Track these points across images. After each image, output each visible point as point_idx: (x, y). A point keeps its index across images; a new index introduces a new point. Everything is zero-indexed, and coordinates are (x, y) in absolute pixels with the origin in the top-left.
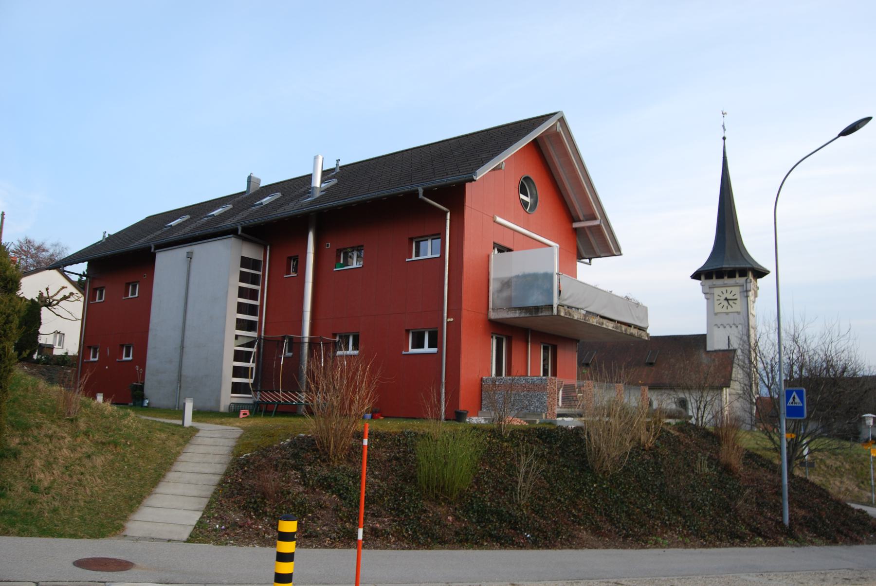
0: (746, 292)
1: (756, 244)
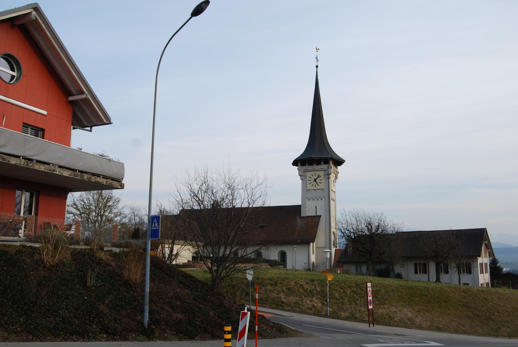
0: (328, 175)
1: (336, 141)
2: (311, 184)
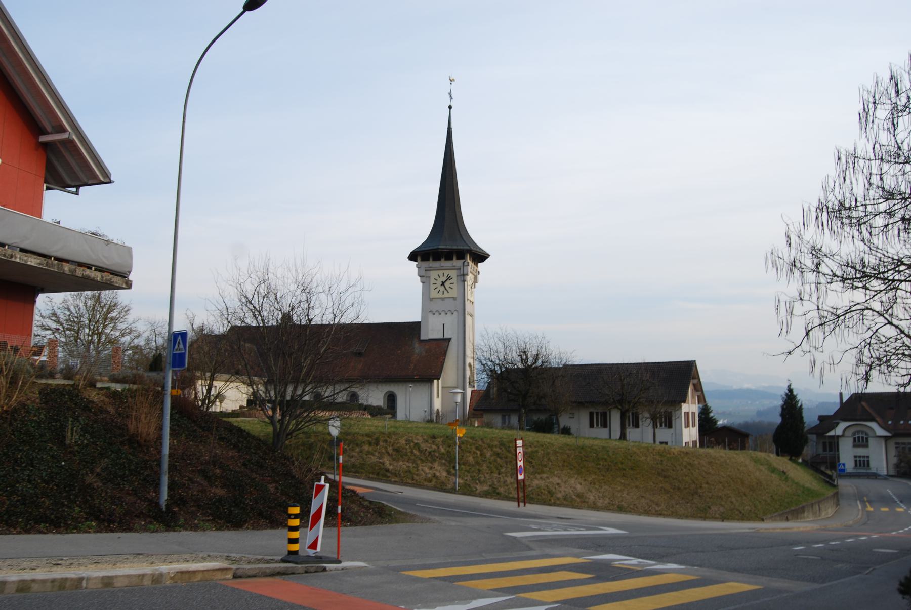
0: (463, 277)
1: (477, 224)
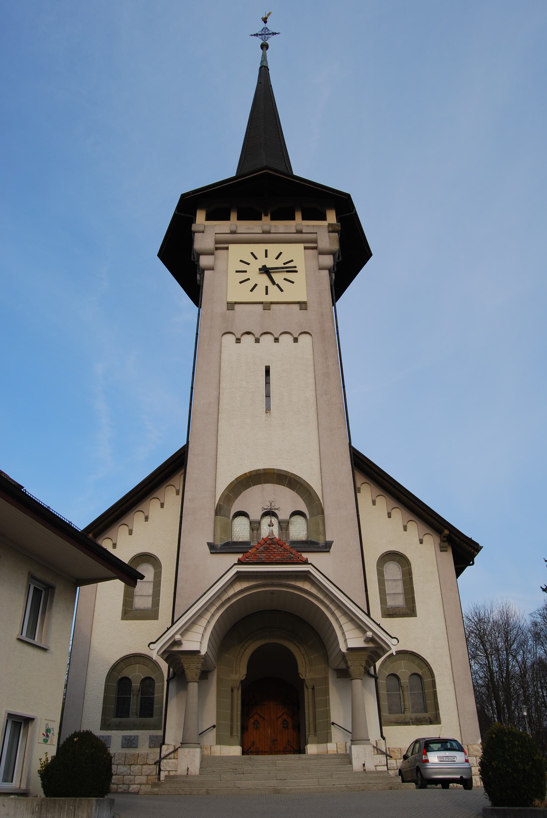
2: (249, 285)
